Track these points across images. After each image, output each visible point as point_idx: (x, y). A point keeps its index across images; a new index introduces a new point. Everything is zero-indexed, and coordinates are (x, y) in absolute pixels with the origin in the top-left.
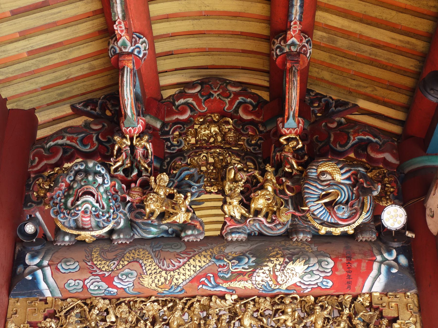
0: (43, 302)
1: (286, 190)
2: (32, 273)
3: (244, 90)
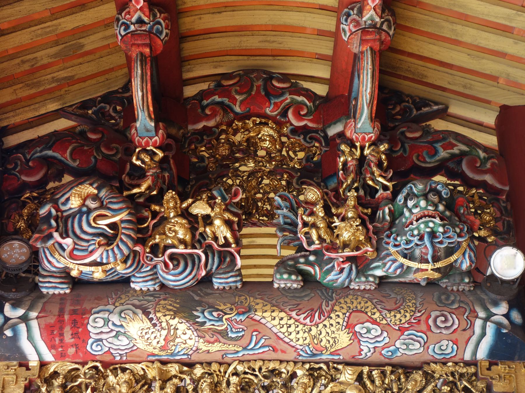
0: (24, 368)
1: (143, 226)
2: (14, 328)
3: (219, 85)
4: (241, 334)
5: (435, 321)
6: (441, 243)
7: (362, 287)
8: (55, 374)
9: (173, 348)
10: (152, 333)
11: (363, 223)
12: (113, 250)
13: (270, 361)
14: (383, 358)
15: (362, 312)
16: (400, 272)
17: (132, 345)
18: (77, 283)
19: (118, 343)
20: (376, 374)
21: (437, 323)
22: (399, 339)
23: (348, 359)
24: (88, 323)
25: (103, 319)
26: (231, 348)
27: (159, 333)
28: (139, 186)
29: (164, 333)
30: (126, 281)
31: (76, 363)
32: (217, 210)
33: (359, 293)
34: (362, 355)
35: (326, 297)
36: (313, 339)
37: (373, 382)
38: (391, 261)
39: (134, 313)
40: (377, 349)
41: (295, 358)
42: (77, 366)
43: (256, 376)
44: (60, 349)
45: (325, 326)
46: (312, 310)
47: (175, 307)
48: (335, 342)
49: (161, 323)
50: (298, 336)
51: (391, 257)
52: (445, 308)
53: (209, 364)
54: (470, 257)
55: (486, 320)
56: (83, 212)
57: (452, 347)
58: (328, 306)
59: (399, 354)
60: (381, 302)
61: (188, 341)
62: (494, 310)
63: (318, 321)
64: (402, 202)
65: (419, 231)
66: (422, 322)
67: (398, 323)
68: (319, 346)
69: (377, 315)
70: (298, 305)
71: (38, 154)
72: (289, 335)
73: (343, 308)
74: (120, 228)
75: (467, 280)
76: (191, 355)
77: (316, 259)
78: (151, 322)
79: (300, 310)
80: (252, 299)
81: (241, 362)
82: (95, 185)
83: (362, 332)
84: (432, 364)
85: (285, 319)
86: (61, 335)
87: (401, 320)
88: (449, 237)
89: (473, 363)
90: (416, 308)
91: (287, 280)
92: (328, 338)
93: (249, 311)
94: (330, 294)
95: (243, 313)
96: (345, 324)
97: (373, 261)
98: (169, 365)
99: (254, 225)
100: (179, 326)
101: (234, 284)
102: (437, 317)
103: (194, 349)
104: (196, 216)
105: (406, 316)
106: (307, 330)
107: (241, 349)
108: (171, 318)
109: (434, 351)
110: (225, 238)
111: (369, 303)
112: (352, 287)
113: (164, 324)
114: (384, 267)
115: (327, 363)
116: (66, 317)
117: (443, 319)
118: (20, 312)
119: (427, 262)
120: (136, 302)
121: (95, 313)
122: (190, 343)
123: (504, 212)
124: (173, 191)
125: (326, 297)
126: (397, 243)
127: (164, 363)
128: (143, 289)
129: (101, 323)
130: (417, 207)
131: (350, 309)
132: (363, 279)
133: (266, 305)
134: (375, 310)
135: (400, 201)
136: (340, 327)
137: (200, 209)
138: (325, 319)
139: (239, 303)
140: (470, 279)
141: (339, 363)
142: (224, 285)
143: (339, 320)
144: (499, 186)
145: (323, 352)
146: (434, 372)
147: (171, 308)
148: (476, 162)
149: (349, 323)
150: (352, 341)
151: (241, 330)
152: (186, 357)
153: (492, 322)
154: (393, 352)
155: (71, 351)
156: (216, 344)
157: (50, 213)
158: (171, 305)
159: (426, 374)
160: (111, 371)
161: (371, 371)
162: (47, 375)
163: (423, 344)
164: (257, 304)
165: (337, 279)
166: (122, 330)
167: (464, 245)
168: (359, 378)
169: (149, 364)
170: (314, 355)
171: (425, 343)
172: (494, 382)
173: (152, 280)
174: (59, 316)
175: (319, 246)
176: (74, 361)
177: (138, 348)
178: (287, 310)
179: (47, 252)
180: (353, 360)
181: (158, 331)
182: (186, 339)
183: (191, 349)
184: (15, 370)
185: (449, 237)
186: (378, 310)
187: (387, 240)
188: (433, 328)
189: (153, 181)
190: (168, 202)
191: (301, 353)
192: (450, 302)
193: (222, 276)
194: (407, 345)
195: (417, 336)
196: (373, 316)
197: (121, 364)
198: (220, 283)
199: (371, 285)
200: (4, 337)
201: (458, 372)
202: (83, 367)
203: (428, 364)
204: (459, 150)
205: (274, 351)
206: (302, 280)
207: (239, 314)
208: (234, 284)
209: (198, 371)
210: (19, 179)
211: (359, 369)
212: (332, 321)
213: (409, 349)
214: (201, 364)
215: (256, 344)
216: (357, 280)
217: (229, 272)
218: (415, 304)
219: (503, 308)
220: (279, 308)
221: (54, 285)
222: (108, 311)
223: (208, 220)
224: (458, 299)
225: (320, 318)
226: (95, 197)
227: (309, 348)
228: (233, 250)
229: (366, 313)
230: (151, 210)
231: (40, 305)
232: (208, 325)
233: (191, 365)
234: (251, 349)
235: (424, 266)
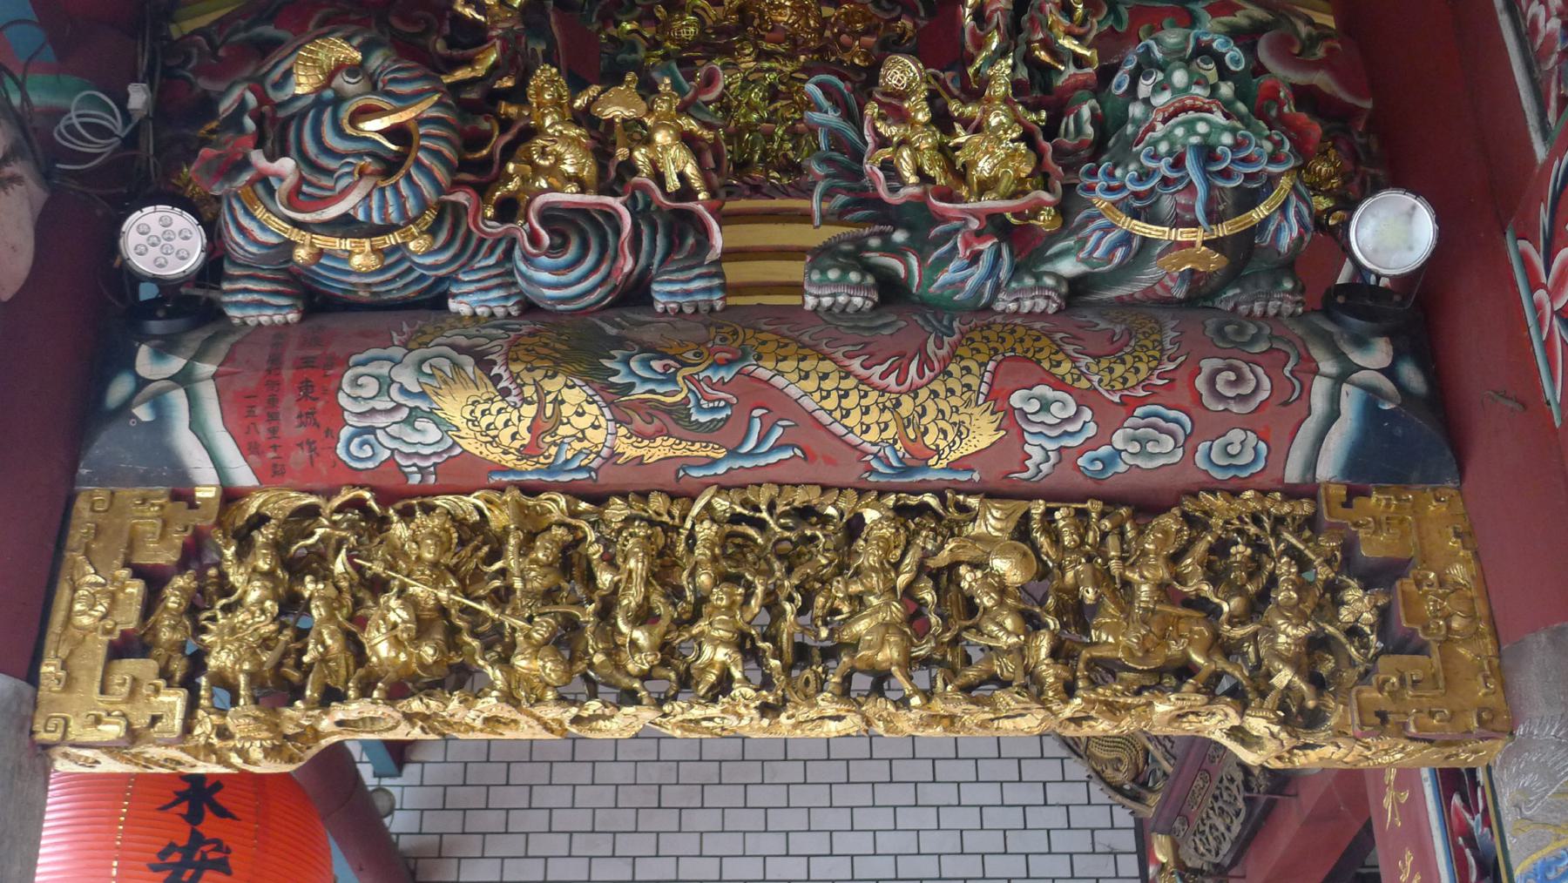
2: (158, 403)
4: (722, 415)
5: (1211, 382)
6: (1226, 174)
7: (1027, 305)
8: (260, 520)
9: (553, 450)
10: (499, 412)
11: (1027, 137)
12: (395, 187)
13: (796, 485)
14: (1080, 478)
15: (1030, 360)
16: (1124, 257)
17: (450, 442)
18: (317, 298)
19: (416, 438)
20: (1063, 518)
21: (1218, 387)
22: (1121, 427)
23: (994, 481)
24: (340, 388)
25: (377, 377)
26: (698, 450)
27: (515, 414)
28: (469, 62)
29: (529, 411)
30: (435, 300)
31: (311, 492)
32: (662, 106)
33: (1018, 321)
34: (1027, 469)
35: (935, 329)
36: (906, 428)
37: (1056, 539)
38: (1100, 229)
39: (456, 365)
40: (1064, 453)
41: (860, 478)
42: (312, 499)
43: (761, 525)
44: (271, 455)
45: (935, 394)
46: (902, 355)
47: (556, 351)
48: (959, 434)
49: (520, 386)
50: (866, 419)
51: (1099, 222)
52: (1236, 352)
53: (644, 496)
54: (1298, 214)
55: (1339, 380)
56: (326, 101)
57: (1255, 448)
58: (940, 348)
59: (1122, 468)
60: (1074, 337)
61: (590, 433)
62: (1357, 357)
63: (917, 381)
64: (1125, 87)
65: (1172, 144)
66: (1178, 383)
67: (1118, 386)
68: (919, 445)
69: (1066, 366)
70: (866, 344)
71: (242, 35)
72: (843, 417)
73: (979, 351)
74: (415, 138)
75: (1288, 285)
76: (596, 471)
77: (910, 239)
78: (495, 386)
79: (871, 355)
80: (749, 332)
81: (723, 489)
82: (356, 42)
83: (1028, 409)
84: (1202, 494)
85: (834, 376)
86: (272, 417)
87: (1125, 380)
88: (1246, 161)
89: (1306, 490)
90: (1162, 351)
91: (836, 283)
92: (942, 424)
93: (744, 357)
94: (945, 322)
95: (728, 363)
96: (984, 388)
97: (1053, 238)
98: (543, 496)
99: (756, 190)
100: (567, 394)
101: (705, 297)
102: (1218, 371)
103: (605, 452)
104: (610, 122)
105: (1137, 371)
106: (888, 404)
107: (722, 453)
108: (546, 376)
109: (1209, 457)
110: (682, 176)
111: (1045, 341)
112: (999, 306)
113: (529, 391)
114: (1082, 249)
115: (940, 494)
116: (287, 374)
117: (1232, 376)
118: (176, 364)
119: (1195, 223)
120: (462, 341)
121: (357, 365)
122: (597, 436)
123: (1363, 157)
124: (553, 66)
125: (935, 329)
126: (1115, 184)
127: (531, 490)
128: (479, 311)
129: (371, 387)
130: (1164, 89)
131: (996, 351)
132: (1029, 281)
133: (786, 345)
134: (1060, 356)
135: (1119, 86)
136: (974, 397)
137: (617, 108)
138: (935, 378)
139: (717, 341)
140: (1296, 284)
141: (969, 493)
142: (680, 300)
143: (968, 379)
144: (1347, 98)
145: (931, 462)
146: (1208, 514)
147: (546, 351)
148: (1292, 43)
149: (996, 387)
150: (1002, 433)
151: (722, 403)
152: (585, 475)
153: (1353, 384)
154: (1107, 462)
155: (300, 456)
156: (659, 440)
157: (242, 102)
158: (546, 345)
159: (1188, 518)
160: (398, 512)
161: (1049, 513)
162: (239, 523)
163: (1181, 439)
164: (764, 343)
165: (964, 281)
166: (424, 406)
167: (1285, 182)
168: (1022, 532)
169: (494, 496)
170: (906, 470)
171: (1187, 437)
172: (1362, 534)
173: (498, 286)
174: (269, 371)
175: (917, 190)
176: (308, 485)
177: (464, 451)
178: (839, 355)
179: (237, 206)
180: (1004, 486)
181: (515, 407)
182: (585, 425)
183: (598, 454)
184: (162, 506)
185: (1246, 161)
186: (1068, 356)
187: (1088, 181)
188: (1207, 400)
189: (503, 51)
190: (540, 91)
191: (875, 464)
192: (1247, 338)
193: (674, 277)
194: (1143, 442)
195: (1167, 420)
196: (1054, 370)
197: (424, 496)
198: (671, 294)
199: (1048, 297)
200: (132, 423)
201: (1269, 514)
202: (329, 500)
203: (1195, 495)
204: (1249, 17)
205: (805, 459)
206: (873, 286)
207: (717, 365)
208: (705, 297)
209: (617, 510)
210: (192, 86)
211: (1022, 506)
212: (952, 383)
213: (1146, 450)
214: (624, 496)
215: (761, 440)
216: (1014, 285)
217: (691, 268)
218: (1161, 343)
219: (1379, 354)
220: (818, 352)
221: (256, 297)
222: (389, 359)
223: (639, 134)
224: (1267, 331)
225: (921, 374)
226: (354, 70)
227: (896, 451)
228: (700, 207)
229: (1039, 362)
230: (497, 116)
231: (223, 348)
232: (639, 392)
233: (599, 499)
234: (750, 454)
235: (1183, 235)
